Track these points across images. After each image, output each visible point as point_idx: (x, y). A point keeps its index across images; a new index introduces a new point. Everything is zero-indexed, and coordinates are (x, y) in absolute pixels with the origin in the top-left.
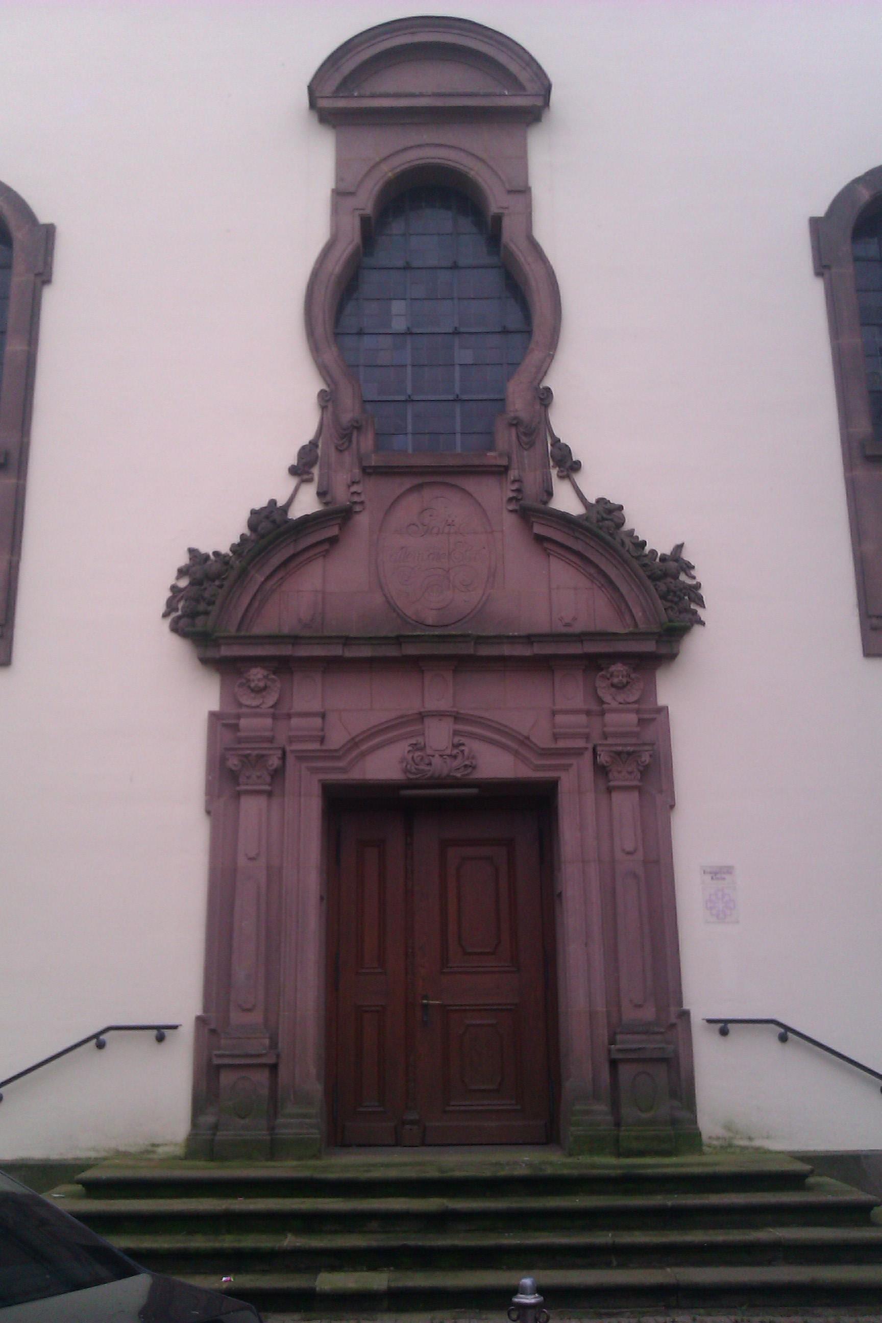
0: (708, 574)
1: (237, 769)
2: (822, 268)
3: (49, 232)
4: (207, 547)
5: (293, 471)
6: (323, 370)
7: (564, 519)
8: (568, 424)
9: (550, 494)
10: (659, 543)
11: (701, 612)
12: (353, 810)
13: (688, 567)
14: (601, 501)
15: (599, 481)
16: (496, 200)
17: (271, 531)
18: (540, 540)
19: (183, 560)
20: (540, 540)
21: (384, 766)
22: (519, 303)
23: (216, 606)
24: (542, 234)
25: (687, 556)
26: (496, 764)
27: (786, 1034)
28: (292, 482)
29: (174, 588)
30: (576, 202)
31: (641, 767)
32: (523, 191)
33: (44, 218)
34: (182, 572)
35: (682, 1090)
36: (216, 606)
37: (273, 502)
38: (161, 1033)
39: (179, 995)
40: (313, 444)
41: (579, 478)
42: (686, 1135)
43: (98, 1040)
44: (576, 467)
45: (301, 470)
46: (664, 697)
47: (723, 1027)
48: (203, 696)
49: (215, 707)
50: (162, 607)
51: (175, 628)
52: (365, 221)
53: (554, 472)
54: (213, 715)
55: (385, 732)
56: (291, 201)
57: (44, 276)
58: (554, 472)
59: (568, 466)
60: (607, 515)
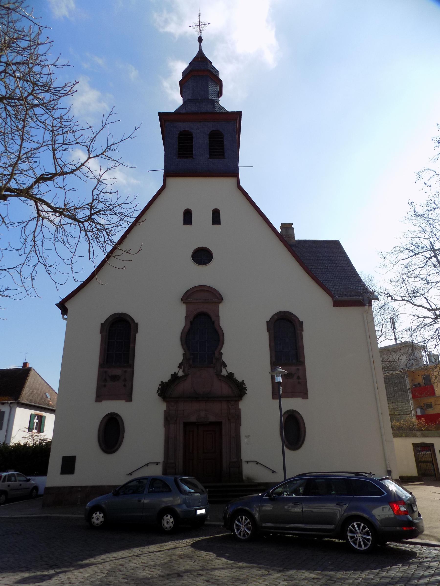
0: (248, 385)
1: (169, 419)
2: (268, 330)
3: (137, 324)
4: (164, 381)
5: (178, 367)
6: (184, 349)
7: (223, 376)
8: (225, 358)
9: (222, 371)
10: (240, 380)
11: (247, 392)
12: (188, 426)
13: (245, 384)
14: (230, 372)
15: (230, 369)
16: (214, 318)
17: (175, 377)
18: (220, 380)
19: (160, 383)
20: (220, 380)
21: (193, 419)
22: (216, 337)
23: (165, 391)
24: (221, 324)
25: (244, 382)
26: (212, 419)
27: (257, 463)
28: (179, 369)
29: (158, 388)
30: (228, 317)
31: (236, 418)
32: (218, 316)
33: (136, 322)
34: (160, 385)
35: (240, 472)
36: (165, 391)
37: (175, 373)
38: (157, 464)
39: (159, 457)
40: (182, 362)
41: (227, 368)
42: (242, 480)
43: (147, 465)
44: (226, 366)
45: (179, 367)
46: (240, 407)
47: (248, 462)
48: (163, 406)
49: (165, 409)
50: (157, 392)
51: (159, 395)
52: (191, 322)
53: (223, 367)
54: (165, 410)
55: (193, 412)
56: (176, 318)
57: (137, 332)
58: (223, 367)
59: (225, 366)
60: (231, 375)
